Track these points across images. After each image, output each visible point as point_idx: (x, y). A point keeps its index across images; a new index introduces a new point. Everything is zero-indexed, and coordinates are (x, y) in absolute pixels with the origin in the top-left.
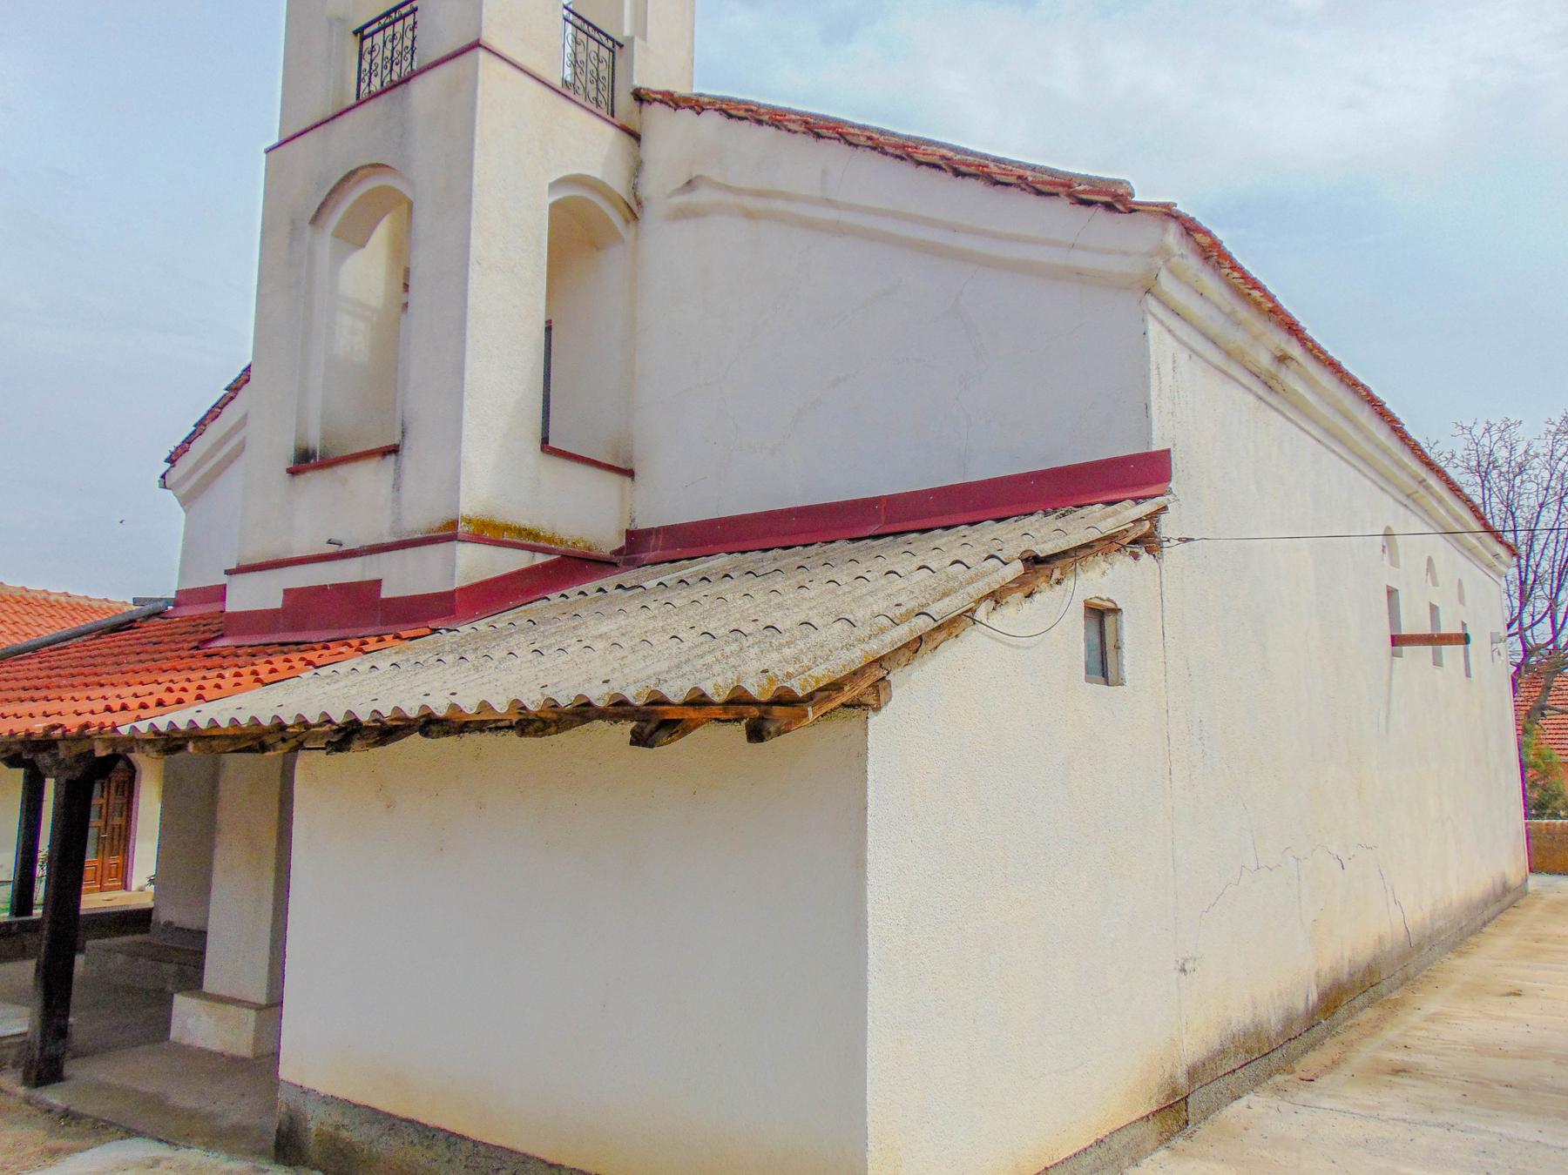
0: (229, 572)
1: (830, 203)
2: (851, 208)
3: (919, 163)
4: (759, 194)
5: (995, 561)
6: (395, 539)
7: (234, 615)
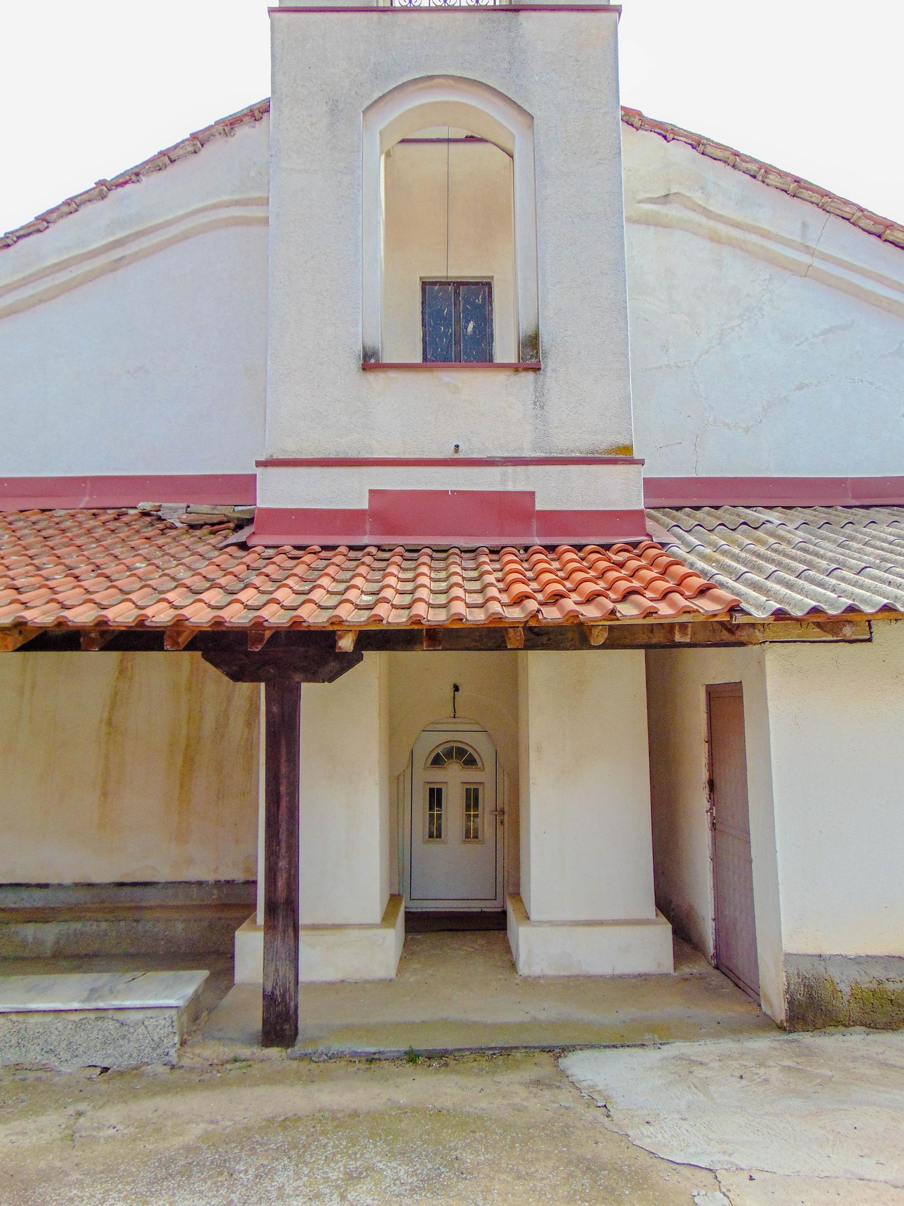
0: (259, 464)
4: (737, 225)
5: (202, 604)
6: (543, 455)
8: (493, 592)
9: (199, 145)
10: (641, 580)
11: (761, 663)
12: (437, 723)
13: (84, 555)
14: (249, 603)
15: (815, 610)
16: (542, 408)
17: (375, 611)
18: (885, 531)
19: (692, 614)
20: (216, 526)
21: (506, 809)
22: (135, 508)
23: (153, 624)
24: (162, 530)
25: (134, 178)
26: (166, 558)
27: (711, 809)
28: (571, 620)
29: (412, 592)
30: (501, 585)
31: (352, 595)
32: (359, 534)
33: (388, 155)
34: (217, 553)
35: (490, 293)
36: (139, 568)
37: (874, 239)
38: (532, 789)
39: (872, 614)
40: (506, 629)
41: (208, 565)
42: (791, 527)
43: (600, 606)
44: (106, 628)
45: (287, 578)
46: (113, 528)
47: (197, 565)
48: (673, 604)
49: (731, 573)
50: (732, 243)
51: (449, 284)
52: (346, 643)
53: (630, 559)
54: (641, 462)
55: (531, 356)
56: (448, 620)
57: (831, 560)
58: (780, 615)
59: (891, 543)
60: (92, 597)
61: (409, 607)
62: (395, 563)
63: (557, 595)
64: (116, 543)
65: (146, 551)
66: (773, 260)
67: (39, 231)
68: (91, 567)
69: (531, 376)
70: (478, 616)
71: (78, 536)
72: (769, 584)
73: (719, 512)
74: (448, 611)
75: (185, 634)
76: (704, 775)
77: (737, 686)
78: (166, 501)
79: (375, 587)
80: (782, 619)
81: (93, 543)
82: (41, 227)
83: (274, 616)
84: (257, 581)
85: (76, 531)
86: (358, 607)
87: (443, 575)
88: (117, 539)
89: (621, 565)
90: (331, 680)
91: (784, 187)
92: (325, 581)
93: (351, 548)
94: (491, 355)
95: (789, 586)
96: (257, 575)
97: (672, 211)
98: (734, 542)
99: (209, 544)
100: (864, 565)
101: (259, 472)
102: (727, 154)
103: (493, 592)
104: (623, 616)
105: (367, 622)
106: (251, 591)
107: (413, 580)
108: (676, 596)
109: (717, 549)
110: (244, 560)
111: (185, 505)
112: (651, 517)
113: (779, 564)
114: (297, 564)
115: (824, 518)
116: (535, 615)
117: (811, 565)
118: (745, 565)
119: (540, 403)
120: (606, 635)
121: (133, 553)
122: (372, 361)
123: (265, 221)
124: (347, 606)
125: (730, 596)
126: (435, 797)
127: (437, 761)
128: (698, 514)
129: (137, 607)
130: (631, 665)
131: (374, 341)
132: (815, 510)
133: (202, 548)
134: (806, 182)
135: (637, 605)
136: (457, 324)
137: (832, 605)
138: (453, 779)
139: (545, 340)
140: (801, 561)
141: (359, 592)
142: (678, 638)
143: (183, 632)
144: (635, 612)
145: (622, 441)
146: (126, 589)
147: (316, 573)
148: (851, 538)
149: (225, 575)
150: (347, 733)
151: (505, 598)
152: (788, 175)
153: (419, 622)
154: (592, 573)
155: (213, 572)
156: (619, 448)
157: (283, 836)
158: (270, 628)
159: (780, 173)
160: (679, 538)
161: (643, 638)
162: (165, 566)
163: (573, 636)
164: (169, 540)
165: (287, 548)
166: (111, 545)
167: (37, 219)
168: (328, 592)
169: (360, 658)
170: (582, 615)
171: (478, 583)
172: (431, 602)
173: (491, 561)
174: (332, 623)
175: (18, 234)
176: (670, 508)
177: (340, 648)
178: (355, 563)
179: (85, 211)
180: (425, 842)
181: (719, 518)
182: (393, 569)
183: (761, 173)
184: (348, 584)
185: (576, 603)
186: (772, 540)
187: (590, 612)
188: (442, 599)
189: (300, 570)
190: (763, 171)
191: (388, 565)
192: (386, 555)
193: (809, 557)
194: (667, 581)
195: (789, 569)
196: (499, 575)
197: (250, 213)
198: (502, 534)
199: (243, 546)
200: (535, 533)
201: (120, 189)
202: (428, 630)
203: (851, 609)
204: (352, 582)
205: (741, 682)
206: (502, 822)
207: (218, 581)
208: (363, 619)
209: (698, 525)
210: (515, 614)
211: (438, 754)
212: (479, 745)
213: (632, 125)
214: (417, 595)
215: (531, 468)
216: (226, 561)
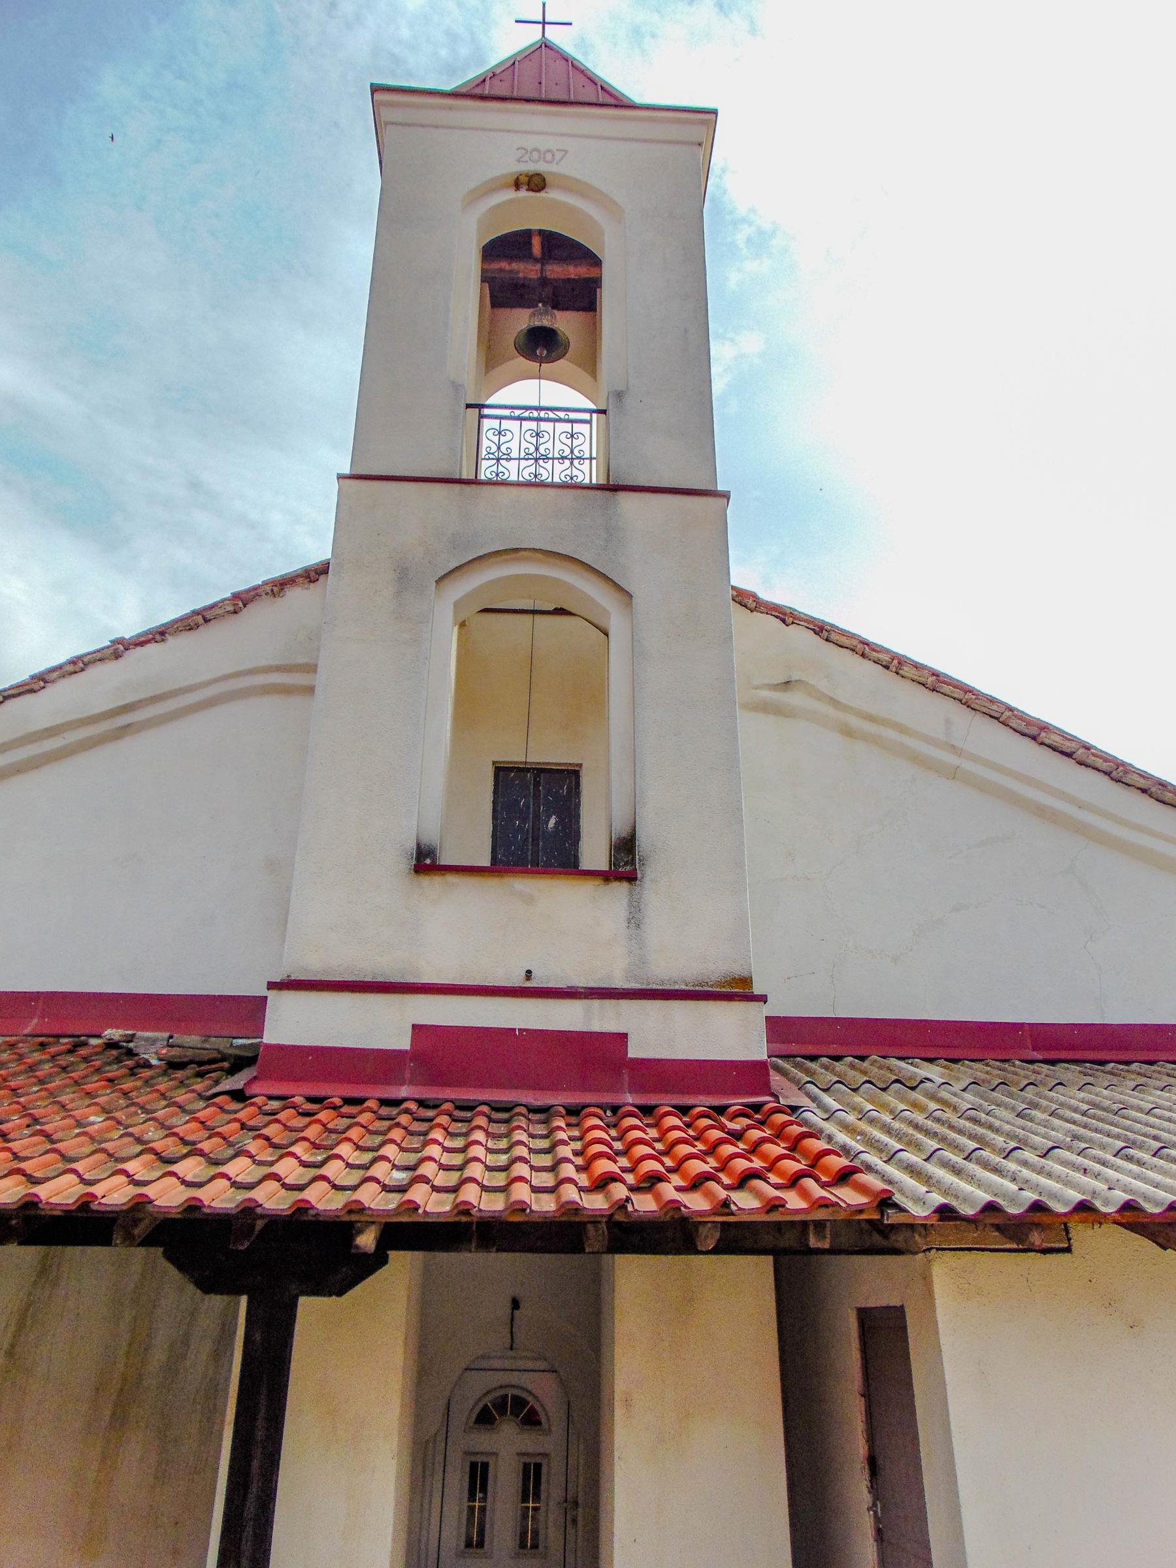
0: (272, 986)
1: (953, 749)
2: (975, 759)
3: (1042, 744)
4: (870, 718)
5: (174, 1179)
6: (638, 986)
7: (269, 1047)
8: (568, 1170)
9: (241, 604)
10: (764, 1157)
11: (927, 1280)
12: (489, 1357)
13: (18, 1103)
14: (238, 1179)
15: (991, 1208)
16: (638, 926)
17: (409, 1196)
18: (1075, 1097)
19: (831, 1209)
20: (204, 1066)
21: (581, 1500)
22: (99, 1036)
23: (103, 1208)
24: (131, 1069)
25: (158, 637)
26: (133, 1109)
27: (875, 1505)
28: (670, 1214)
29: (461, 1168)
30: (579, 1161)
31: (380, 1170)
32: (396, 1084)
33: (463, 625)
34: (202, 1104)
35: (578, 784)
36: (93, 1123)
37: (1027, 741)
38: (617, 1467)
39: (1065, 1214)
40: (584, 1224)
41: (187, 1122)
42: (957, 1087)
43: (709, 1195)
44: (32, 1212)
45: (293, 1144)
46: (63, 1063)
47: (174, 1121)
48: (805, 1194)
49: (881, 1151)
50: (866, 738)
51: (528, 770)
52: (367, 1240)
53: (749, 1127)
54: (763, 999)
55: (625, 863)
56: (506, 1209)
57: (1010, 1136)
58: (945, 1212)
59: (1084, 1114)
60: (23, 1165)
61: (455, 1190)
62: (440, 1125)
63: (652, 1177)
64: (66, 1086)
65: (105, 1098)
66: (917, 759)
67: (33, 691)
68: (26, 1121)
69: (625, 885)
70: (546, 1205)
71: (15, 1075)
72: (933, 1169)
73: (866, 1064)
74: (508, 1197)
75: (147, 1221)
76: (860, 1448)
77: (899, 1312)
78: (142, 1030)
79: (412, 1158)
80: (950, 1219)
81: (35, 1085)
82: (36, 687)
83: (272, 1200)
84: (253, 1146)
85: (13, 1067)
86: (387, 1189)
87: (503, 1144)
88: (68, 1081)
89: (738, 1136)
90: (340, 1294)
91: (922, 680)
92: (345, 1149)
93: (384, 1102)
94: (576, 858)
95: (957, 1171)
96: (254, 1138)
97: (794, 699)
98: (885, 1106)
99: (193, 1091)
100: (1051, 1144)
101: (272, 995)
102: (855, 642)
103: (568, 1170)
104: (740, 1209)
105: (396, 1211)
106: (243, 1161)
107: (463, 1150)
108: (809, 1183)
109: (863, 1115)
110: (239, 1115)
111: (166, 1035)
112: (778, 1069)
113: (943, 1139)
114: (310, 1124)
115: (998, 1076)
116: (622, 1205)
117: (983, 1143)
118: (900, 1140)
119: (635, 920)
120: (717, 1235)
121: (87, 1102)
122: (428, 861)
123: (310, 690)
124: (373, 1187)
125: (878, 1184)
126: (479, 1476)
127: (485, 1418)
128: (839, 1066)
129: (83, 1181)
130: (756, 1273)
131: (432, 836)
132: (987, 1065)
133: (182, 1097)
134: (946, 675)
135: (758, 1194)
136: (535, 822)
137: (1013, 1200)
138: (507, 1445)
139: (644, 842)
140: (972, 1137)
141: (389, 1165)
142: (813, 1242)
143: (140, 1220)
144: (755, 1204)
145: (737, 970)
146: (71, 1154)
147: (334, 1136)
148: (1034, 1105)
149: (209, 1138)
150: (357, 1370)
151: (583, 1180)
152: (924, 667)
153: (467, 1213)
154: (701, 1146)
155: (194, 1132)
156: (734, 979)
157: (247, 1547)
158: (262, 1216)
159: (917, 666)
160: (814, 1099)
161: (768, 1240)
162: (129, 1121)
163: (671, 1235)
164: (139, 1083)
165: (298, 1100)
166: (59, 1087)
167: (33, 677)
168: (348, 1165)
169: (384, 1261)
170: (686, 1207)
171: (549, 1156)
172: (486, 1183)
173: (568, 1125)
174: (350, 1212)
175: (6, 694)
176: (803, 1057)
177: (357, 1247)
178: (387, 1123)
179: (94, 672)
180: (460, 1555)
181: (864, 1073)
182: (437, 1134)
183: (895, 664)
184: (376, 1154)
185: (679, 1189)
186: (933, 1106)
187: (696, 1203)
188: (500, 1179)
189: (313, 1132)
190: (895, 662)
191: (431, 1128)
192: (430, 1113)
193: (980, 1130)
194: (798, 1161)
195: (957, 1148)
196: (578, 1145)
197: (294, 679)
198: (585, 1089)
199: (239, 1096)
200: (626, 1086)
201: (139, 649)
202: (478, 1223)
203: (1037, 1207)
204: (382, 1152)
205: (902, 1306)
206: (574, 1521)
207: (199, 1146)
208: (392, 1206)
209: (838, 1082)
210: (596, 1203)
211: (486, 1405)
212: (544, 1391)
213: (745, 606)
214: (468, 1173)
215: (625, 1004)
216: (214, 1115)
